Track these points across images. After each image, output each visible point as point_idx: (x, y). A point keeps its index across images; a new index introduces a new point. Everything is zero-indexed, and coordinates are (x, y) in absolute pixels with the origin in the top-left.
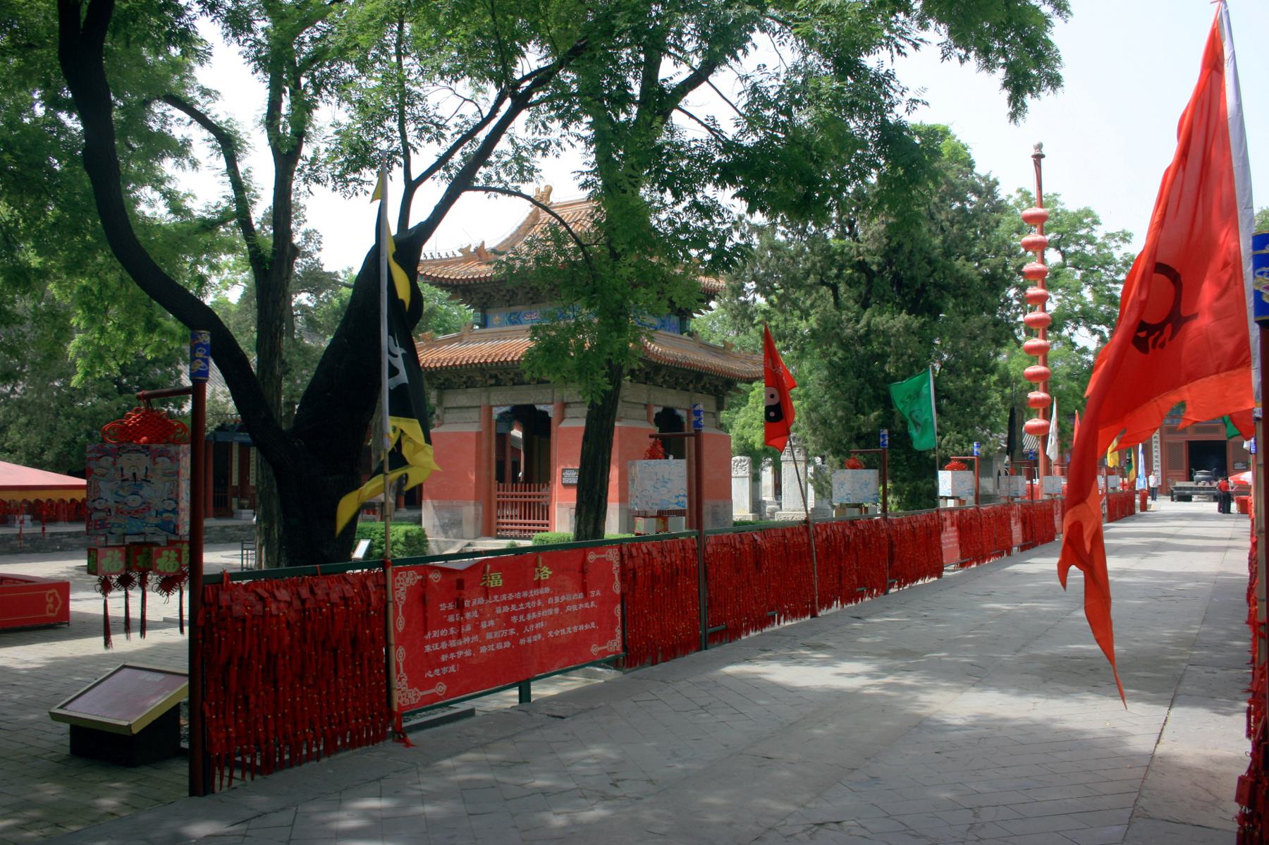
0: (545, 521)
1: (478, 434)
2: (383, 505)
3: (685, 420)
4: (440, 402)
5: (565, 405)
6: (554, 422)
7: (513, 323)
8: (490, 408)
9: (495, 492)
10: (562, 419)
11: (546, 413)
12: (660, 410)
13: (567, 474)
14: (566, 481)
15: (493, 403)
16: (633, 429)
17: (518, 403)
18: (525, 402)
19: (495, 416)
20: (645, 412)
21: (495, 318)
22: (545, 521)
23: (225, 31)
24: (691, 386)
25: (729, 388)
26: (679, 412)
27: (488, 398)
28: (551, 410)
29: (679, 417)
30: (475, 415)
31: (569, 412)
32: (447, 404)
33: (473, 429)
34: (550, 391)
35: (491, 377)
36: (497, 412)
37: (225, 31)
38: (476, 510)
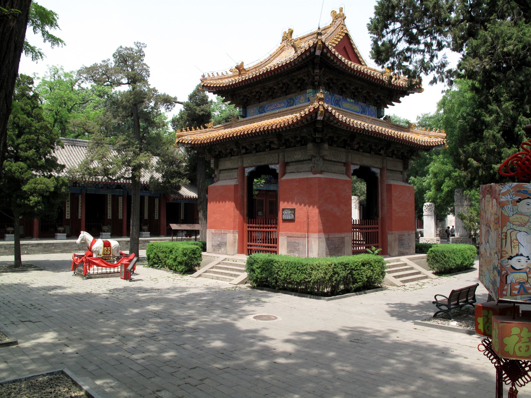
0: (275, 245)
1: (236, 186)
2: (399, 235)
3: (379, 175)
4: (217, 166)
5: (286, 164)
6: (279, 176)
7: (260, 113)
8: (244, 168)
9: (379, 231)
10: (284, 174)
11: (275, 170)
12: (357, 167)
13: (285, 212)
14: (285, 217)
15: (245, 166)
16: (332, 180)
17: (259, 164)
18: (262, 164)
19: (246, 174)
20: (344, 168)
21: (250, 110)
22: (275, 245)
23: (421, 116)
24: (382, 152)
25: (412, 155)
26: (374, 170)
27: (242, 162)
28: (277, 167)
29: (374, 174)
30: (235, 174)
31: (289, 168)
32: (221, 168)
33: (232, 182)
34: (277, 155)
35: (243, 148)
36: (248, 170)
37: (421, 116)
38: (235, 236)
